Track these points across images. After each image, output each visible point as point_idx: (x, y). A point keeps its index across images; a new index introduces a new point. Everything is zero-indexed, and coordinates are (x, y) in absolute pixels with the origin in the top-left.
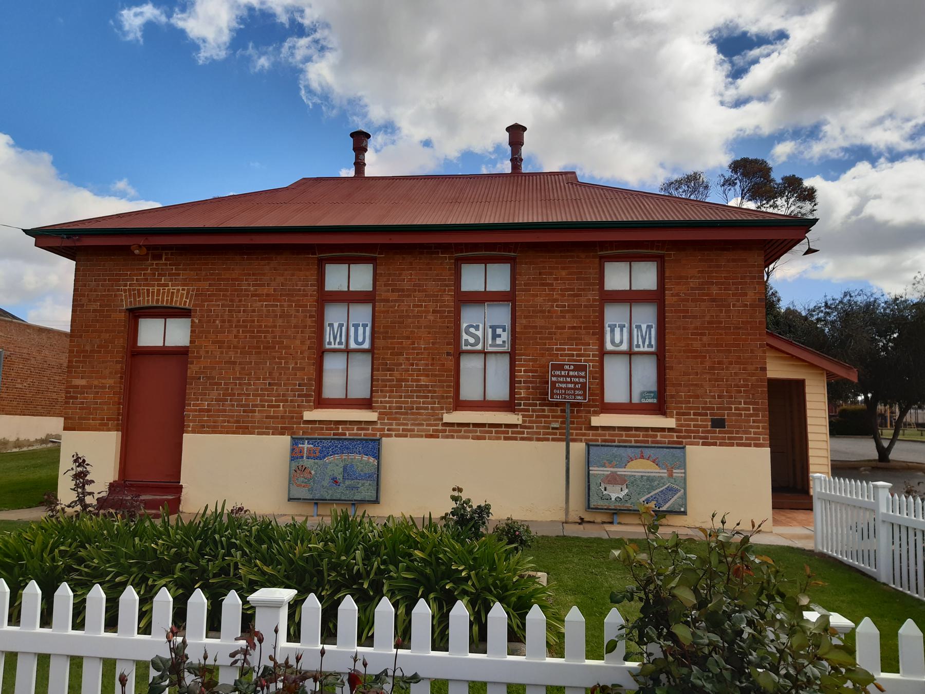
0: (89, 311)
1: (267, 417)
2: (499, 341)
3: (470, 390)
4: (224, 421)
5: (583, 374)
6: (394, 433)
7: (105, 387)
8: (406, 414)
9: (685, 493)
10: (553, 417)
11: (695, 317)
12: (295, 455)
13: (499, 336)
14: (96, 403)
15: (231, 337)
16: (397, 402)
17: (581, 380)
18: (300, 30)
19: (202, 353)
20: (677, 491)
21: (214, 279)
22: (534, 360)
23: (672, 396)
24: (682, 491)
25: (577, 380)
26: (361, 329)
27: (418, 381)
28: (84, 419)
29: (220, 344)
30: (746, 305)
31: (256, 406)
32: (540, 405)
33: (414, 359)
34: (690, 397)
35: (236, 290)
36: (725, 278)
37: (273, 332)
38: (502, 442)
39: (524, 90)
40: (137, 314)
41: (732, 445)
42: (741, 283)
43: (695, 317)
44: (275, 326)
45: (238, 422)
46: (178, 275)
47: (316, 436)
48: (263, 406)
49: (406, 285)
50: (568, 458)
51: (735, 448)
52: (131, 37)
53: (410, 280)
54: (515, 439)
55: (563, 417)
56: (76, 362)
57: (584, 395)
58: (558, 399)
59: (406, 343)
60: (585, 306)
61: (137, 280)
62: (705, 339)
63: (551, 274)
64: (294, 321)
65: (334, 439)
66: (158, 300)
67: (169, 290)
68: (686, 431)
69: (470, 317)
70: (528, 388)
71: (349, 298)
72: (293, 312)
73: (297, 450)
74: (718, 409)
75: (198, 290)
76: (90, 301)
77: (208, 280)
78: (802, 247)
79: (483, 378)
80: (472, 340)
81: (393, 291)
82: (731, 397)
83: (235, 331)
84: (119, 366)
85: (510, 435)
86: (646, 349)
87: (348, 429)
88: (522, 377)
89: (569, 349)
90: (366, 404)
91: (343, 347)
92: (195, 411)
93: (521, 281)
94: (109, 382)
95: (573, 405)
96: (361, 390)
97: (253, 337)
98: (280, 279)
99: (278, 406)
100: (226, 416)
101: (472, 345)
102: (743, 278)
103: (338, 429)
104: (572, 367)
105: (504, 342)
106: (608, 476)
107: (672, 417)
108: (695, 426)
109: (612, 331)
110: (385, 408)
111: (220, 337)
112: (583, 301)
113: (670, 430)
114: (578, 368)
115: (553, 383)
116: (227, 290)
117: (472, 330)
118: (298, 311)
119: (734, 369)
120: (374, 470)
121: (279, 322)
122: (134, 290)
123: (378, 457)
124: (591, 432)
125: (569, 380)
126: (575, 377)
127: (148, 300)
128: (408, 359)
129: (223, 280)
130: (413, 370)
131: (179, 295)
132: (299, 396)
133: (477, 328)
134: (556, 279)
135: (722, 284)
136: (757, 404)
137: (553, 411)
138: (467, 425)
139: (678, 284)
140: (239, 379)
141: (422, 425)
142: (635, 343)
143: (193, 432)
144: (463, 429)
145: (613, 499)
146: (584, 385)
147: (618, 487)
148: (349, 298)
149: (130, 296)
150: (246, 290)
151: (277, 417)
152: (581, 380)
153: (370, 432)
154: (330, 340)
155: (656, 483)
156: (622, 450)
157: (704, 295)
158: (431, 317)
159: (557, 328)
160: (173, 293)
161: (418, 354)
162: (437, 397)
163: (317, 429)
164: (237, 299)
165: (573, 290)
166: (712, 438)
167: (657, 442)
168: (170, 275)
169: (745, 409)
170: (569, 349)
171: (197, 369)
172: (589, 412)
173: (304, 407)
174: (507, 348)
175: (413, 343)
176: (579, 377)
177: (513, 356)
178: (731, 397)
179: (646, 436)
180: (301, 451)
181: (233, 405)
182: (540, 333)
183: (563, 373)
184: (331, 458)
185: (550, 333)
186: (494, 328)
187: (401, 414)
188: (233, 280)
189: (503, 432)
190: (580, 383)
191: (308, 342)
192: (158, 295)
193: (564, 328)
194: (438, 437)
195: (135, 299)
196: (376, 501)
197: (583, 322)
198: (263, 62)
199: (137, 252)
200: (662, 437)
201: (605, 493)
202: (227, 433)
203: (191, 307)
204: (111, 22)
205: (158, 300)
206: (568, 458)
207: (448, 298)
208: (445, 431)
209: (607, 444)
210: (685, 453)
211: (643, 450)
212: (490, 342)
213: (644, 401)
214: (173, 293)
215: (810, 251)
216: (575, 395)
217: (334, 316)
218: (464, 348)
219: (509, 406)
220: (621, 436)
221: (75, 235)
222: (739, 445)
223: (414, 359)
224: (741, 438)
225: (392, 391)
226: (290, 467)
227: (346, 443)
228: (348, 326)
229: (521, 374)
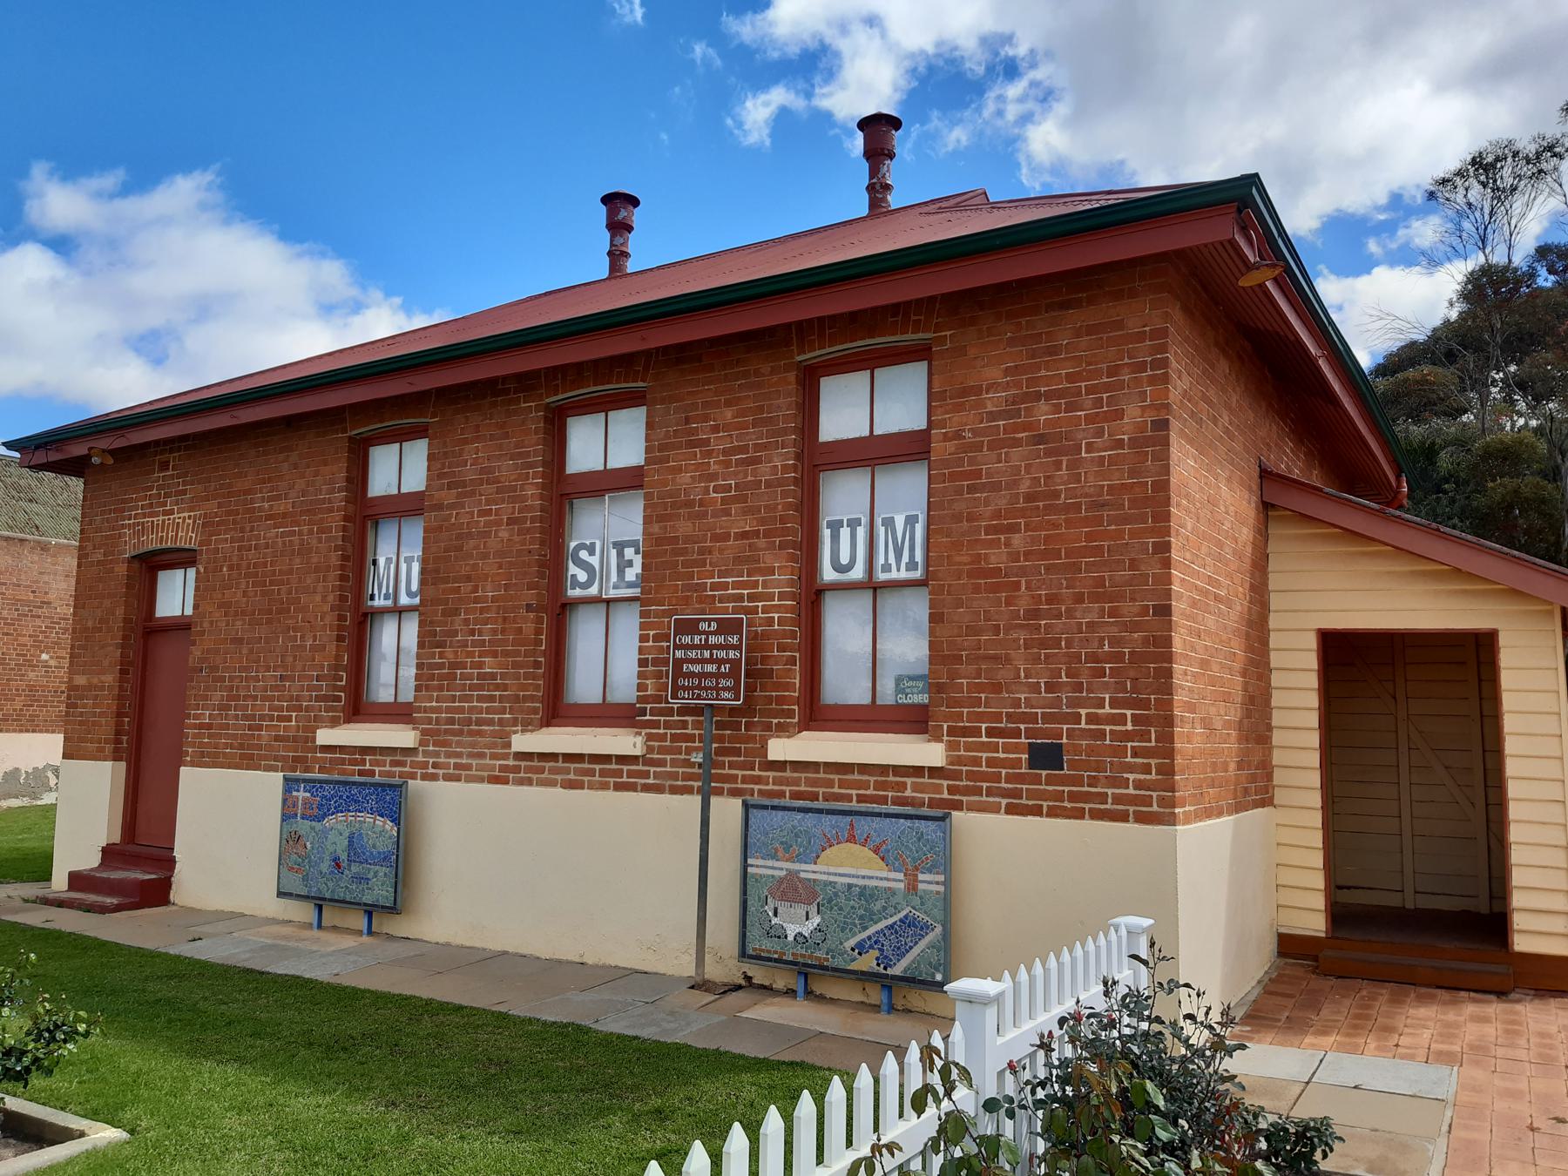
1: (277, 738)
4: (226, 746)
5: (734, 640)
8: (461, 733)
9: (946, 936)
17: (732, 654)
18: (1011, 70)
20: (926, 928)
24: (939, 929)
25: (722, 654)
27: (480, 665)
31: (262, 718)
34: (980, 688)
36: (1071, 378)
39: (1442, 85)
41: (1078, 814)
42: (1107, 387)
43: (995, 487)
46: (184, 492)
51: (1088, 824)
52: (753, 138)
57: (735, 689)
59: (466, 587)
60: (769, 484)
62: (1017, 540)
63: (706, 418)
68: (971, 776)
73: (289, 802)
74: (1047, 718)
80: (582, 576)
82: (1078, 687)
86: (904, 575)
89: (737, 585)
90: (912, 720)
103: (363, 762)
104: (714, 625)
106: (781, 880)
107: (938, 739)
109: (835, 538)
112: (764, 472)
113: (934, 772)
115: (678, 663)
117: (584, 554)
119: (1088, 614)
124: (771, 774)
125: (707, 654)
126: (719, 647)
128: (466, 621)
134: (715, 429)
136: (1145, 704)
139: (959, 408)
142: (881, 561)
143: (193, 764)
145: (790, 938)
146: (735, 663)
147: (800, 910)
152: (732, 654)
155: (878, 906)
159: (715, 538)
161: (482, 610)
166: (1032, 795)
169: (1113, 719)
170: (737, 585)
172: (768, 727)
178: (1078, 687)
179: (814, 783)
182: (684, 552)
185: (702, 551)
186: (620, 546)
190: (728, 661)
191: (331, 598)
194: (507, 783)
196: (393, 909)
197: (762, 521)
198: (958, 136)
200: (916, 788)
204: (729, 122)
211: (855, 818)
212: (614, 578)
213: (903, 700)
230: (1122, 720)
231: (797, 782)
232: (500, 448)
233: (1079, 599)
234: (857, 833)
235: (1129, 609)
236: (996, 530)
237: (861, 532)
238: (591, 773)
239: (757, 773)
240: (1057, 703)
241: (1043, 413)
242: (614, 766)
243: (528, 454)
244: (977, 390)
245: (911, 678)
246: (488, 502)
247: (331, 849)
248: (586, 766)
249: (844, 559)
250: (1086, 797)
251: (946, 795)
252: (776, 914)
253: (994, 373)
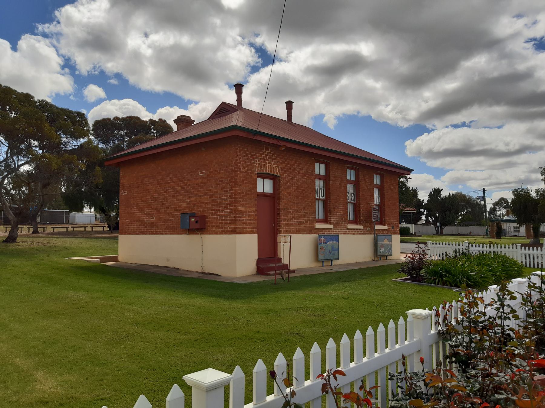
45: (297, 229)
46: (275, 159)
94: (253, 209)
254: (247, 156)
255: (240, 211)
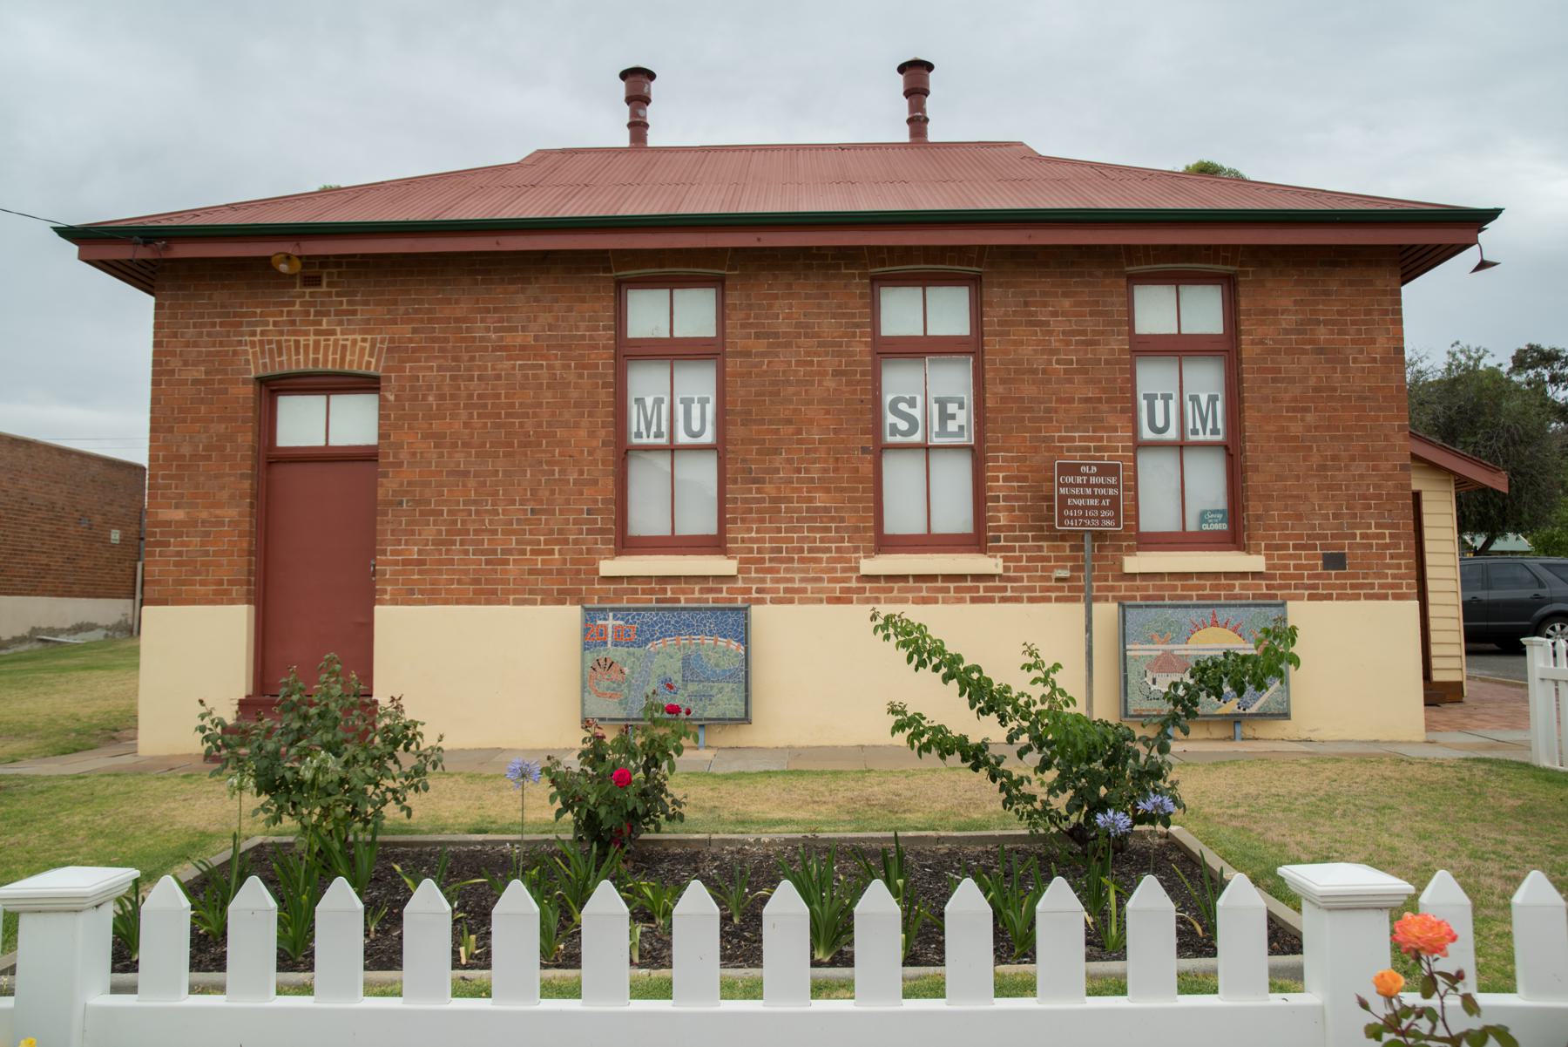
0: (183, 382)
1: (532, 572)
2: (952, 426)
3: (902, 515)
5: (1113, 480)
6: (768, 597)
7: (222, 524)
10: (1057, 559)
11: (1292, 381)
12: (591, 638)
13: (953, 417)
14: (207, 553)
15: (458, 425)
16: (772, 540)
17: (1111, 492)
19: (404, 455)
21: (422, 321)
22: (1022, 459)
23: (1258, 518)
25: (1103, 491)
26: (1159, 404)
27: (810, 500)
28: (184, 583)
29: (438, 438)
30: (1374, 360)
32: (1035, 539)
33: (801, 460)
34: (1288, 517)
35: (463, 340)
36: (1339, 313)
37: (535, 415)
38: (968, 608)
40: (274, 386)
41: (1357, 597)
43: (1292, 381)
44: (540, 405)
45: (476, 581)
46: (354, 313)
47: (625, 605)
48: (523, 552)
49: (782, 325)
50: (1089, 629)
51: (1363, 603)
53: (789, 316)
54: (991, 600)
55: (1075, 559)
56: (164, 477)
57: (1116, 518)
58: (1071, 526)
60: (1107, 362)
61: (275, 323)
62: (1310, 417)
63: (1045, 305)
64: (574, 394)
65: (663, 608)
66: (316, 361)
67: (336, 341)
68: (1283, 577)
69: (900, 383)
70: (1011, 509)
71: (673, 352)
72: (571, 377)
74: (1333, 537)
75: (392, 340)
76: (186, 363)
77: (411, 321)
78: (1470, 257)
79: (928, 494)
80: (903, 425)
81: (757, 336)
82: (1354, 516)
83: (463, 414)
84: (246, 484)
85: (981, 593)
86: (1209, 437)
87: (684, 592)
88: (1000, 489)
89: (1082, 439)
90: (714, 545)
91: (664, 441)
92: (396, 563)
93: (993, 316)
94: (230, 513)
95: (1098, 536)
96: (700, 519)
97: (497, 426)
98: (545, 318)
99: (551, 552)
100: (454, 572)
101: (903, 434)
102: (1368, 312)
103: (665, 591)
104: (1094, 469)
105: (961, 428)
107: (1258, 552)
108: (1296, 567)
110: (751, 550)
111: (436, 426)
112: (1103, 352)
114: (1104, 470)
115: (1063, 498)
116: (446, 340)
117: (903, 407)
118: (581, 376)
119: (1359, 468)
120: (738, 664)
121: (548, 397)
122: (270, 342)
123: (745, 640)
124: (1123, 584)
125: (1089, 491)
126: (1100, 486)
127: (298, 361)
129: (438, 321)
130: (800, 480)
131: (352, 347)
132: (589, 532)
133: (912, 403)
135: (1334, 323)
136: (1396, 526)
137: (1058, 548)
138: (904, 578)
140: (475, 502)
141: (820, 580)
142: (1190, 426)
143: (394, 602)
144: (896, 586)
148: (673, 352)
149: (263, 352)
150: (482, 339)
151: (550, 572)
152: (1111, 492)
153: (724, 595)
154: (639, 429)
156: (1180, 613)
157: (1305, 342)
158: (830, 383)
159: (1060, 400)
160: (344, 347)
161: (808, 451)
162: (846, 529)
163: (625, 591)
164: (466, 356)
165: (1084, 333)
166: (1325, 587)
167: (1235, 597)
168: (338, 313)
170: (1082, 439)
171: (395, 486)
172: (1119, 548)
173: (600, 552)
174: (968, 439)
175: (799, 432)
176: (1107, 486)
177: (978, 455)
178: (1354, 516)
179: (1217, 587)
180: (603, 632)
181: (466, 552)
182: (1030, 410)
183: (1079, 480)
184: (659, 644)
185: (1048, 410)
187: (781, 561)
188: (457, 320)
189: (969, 589)
190: (1108, 497)
191: (602, 433)
192: (316, 350)
193: (1070, 400)
195: (272, 359)
197: (1104, 390)
199: (284, 268)
200: (1243, 587)
201: (1153, 688)
202: (458, 602)
203: (380, 373)
205: (316, 361)
206: (1089, 629)
207: (860, 348)
208: (862, 590)
209: (1152, 602)
210: (1285, 613)
211: (1217, 610)
212: (936, 428)
213: (1205, 527)
214: (344, 347)
215: (1483, 265)
216: (1099, 518)
217: (647, 385)
218: (890, 439)
219: (976, 541)
220: (1174, 588)
221: (160, 238)
222: (1368, 597)
223: (801, 460)
224: (1372, 586)
225: (762, 521)
226: (583, 661)
227: (685, 615)
228: (674, 404)
229: (999, 484)
230: (1382, 536)
231: (1146, 588)
232: (819, 306)
233: (1353, 459)
234: (1219, 619)
235: (1385, 466)
236: (1294, 410)
237: (1173, 405)
238: (947, 590)
239: (1110, 583)
240: (1340, 526)
241: (1322, 334)
242: (969, 584)
243: (853, 315)
244: (1275, 313)
245: (1213, 512)
246: (808, 354)
247: (659, 672)
248: (939, 584)
249: (1160, 423)
250: (1362, 586)
251: (1265, 591)
252: (1154, 682)
253: (1286, 302)
254: (202, 325)
255: (168, 523)
